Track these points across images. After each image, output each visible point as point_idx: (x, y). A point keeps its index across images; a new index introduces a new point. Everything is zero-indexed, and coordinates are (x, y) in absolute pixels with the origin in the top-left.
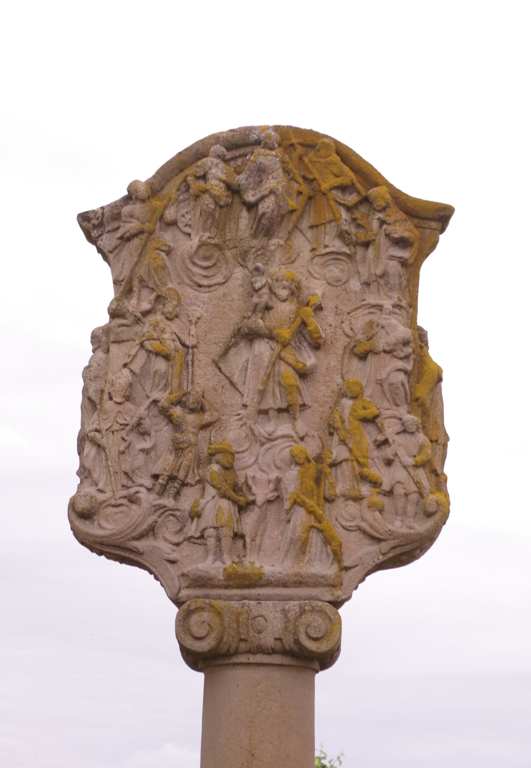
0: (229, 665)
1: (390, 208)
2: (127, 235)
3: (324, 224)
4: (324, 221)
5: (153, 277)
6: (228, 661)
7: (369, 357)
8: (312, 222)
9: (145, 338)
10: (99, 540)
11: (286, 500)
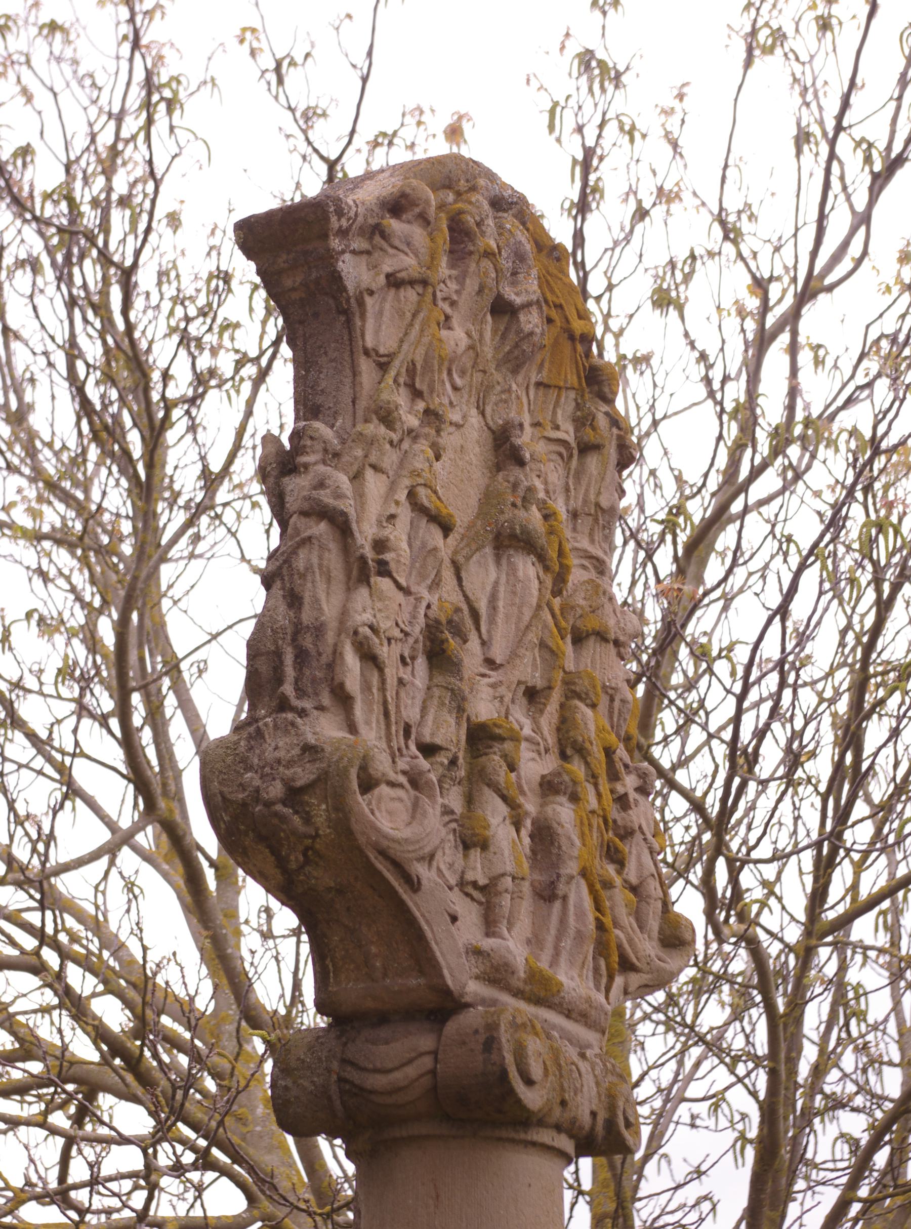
0: (513, 1141)
1: (829, 486)
2: (403, 275)
3: (560, 388)
4: (562, 384)
5: (433, 371)
6: (522, 1136)
7: (592, 641)
8: (544, 376)
9: (422, 481)
10: (385, 843)
11: (571, 858)
